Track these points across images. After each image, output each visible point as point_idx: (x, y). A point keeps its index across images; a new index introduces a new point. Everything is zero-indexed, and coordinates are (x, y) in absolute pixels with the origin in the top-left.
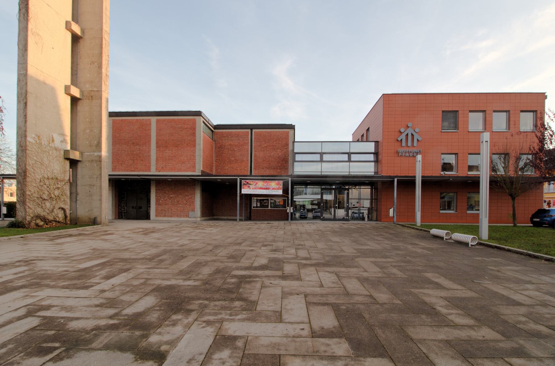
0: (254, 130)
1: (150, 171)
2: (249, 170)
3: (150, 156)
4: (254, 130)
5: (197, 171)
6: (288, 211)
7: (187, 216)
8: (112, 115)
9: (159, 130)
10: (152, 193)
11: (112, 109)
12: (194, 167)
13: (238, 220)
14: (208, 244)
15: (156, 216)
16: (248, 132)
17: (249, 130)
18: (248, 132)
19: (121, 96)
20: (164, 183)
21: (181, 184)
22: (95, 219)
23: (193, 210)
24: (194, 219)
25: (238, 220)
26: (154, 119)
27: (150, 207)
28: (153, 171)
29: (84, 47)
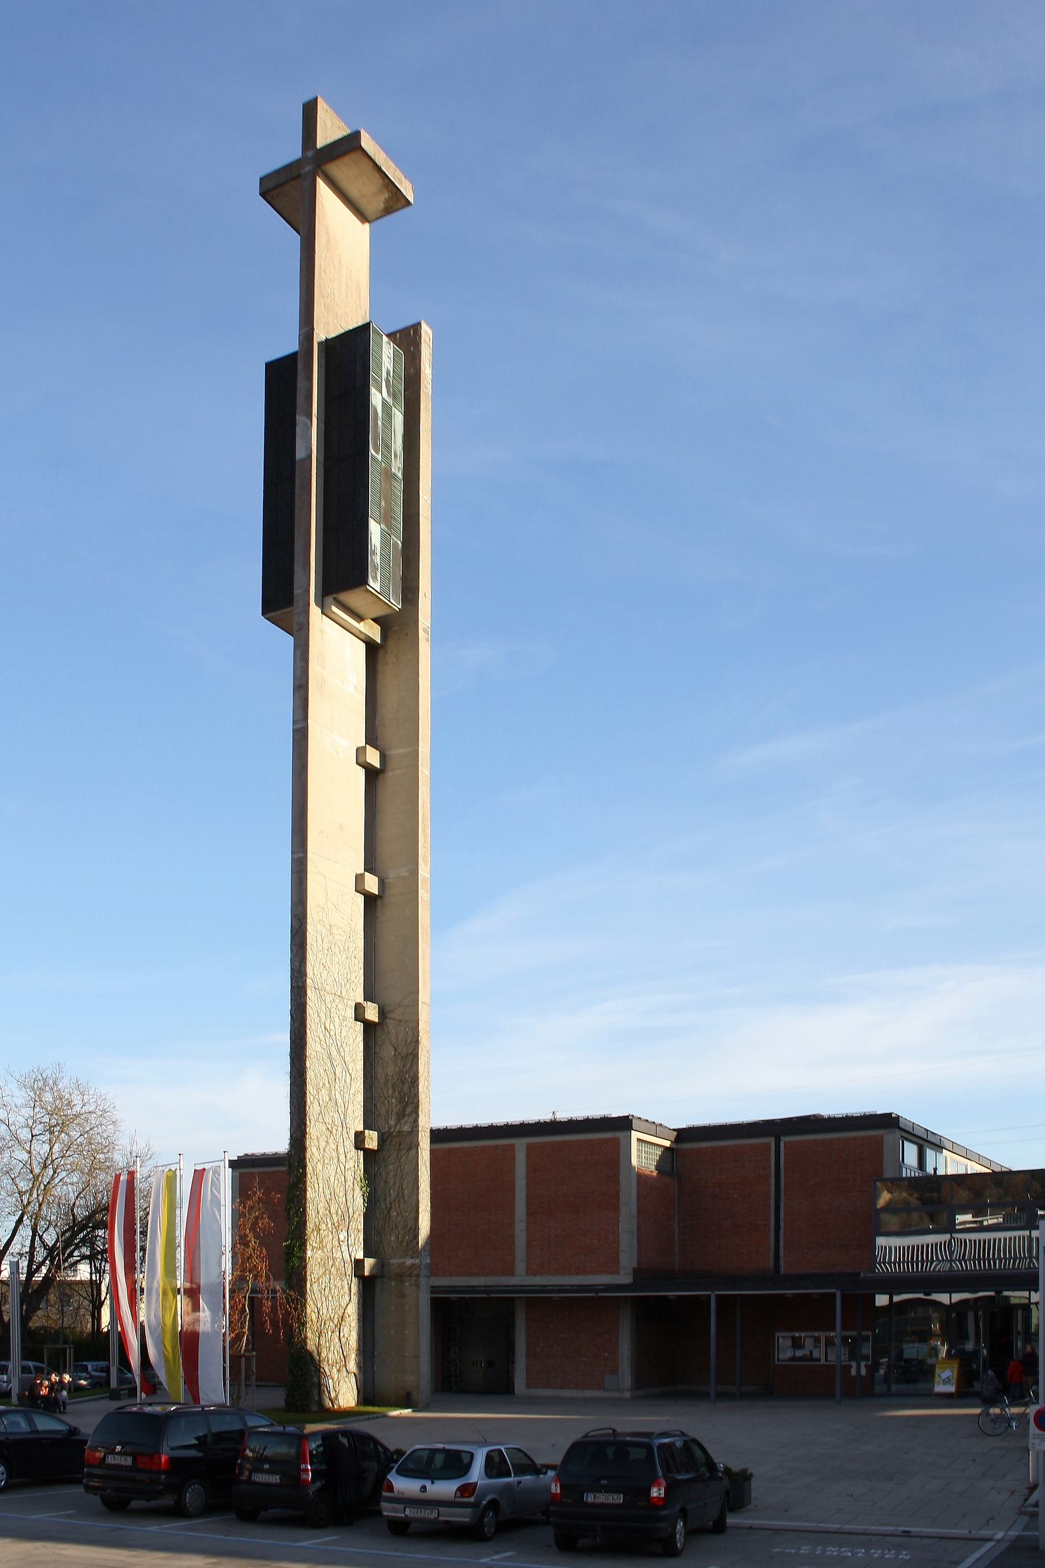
0: (784, 1139)
1: (511, 1272)
2: (772, 1253)
3: (513, 1236)
4: (784, 1139)
5: (622, 1271)
6: (853, 1372)
7: (600, 1386)
8: (438, 1135)
9: (532, 1170)
10: (517, 1328)
11: (440, 1123)
12: (616, 1260)
13: (712, 1396)
14: (30, 1152)
15: (528, 1385)
16: (767, 1146)
17: (772, 1140)
18: (767, 1146)
19: (459, 1091)
20: (543, 1304)
21: (589, 1307)
22: (409, 1395)
23: (615, 1371)
24: (617, 1394)
25: (712, 1396)
26: (520, 1145)
27: (513, 1362)
28: (520, 1278)
29: (388, 915)
